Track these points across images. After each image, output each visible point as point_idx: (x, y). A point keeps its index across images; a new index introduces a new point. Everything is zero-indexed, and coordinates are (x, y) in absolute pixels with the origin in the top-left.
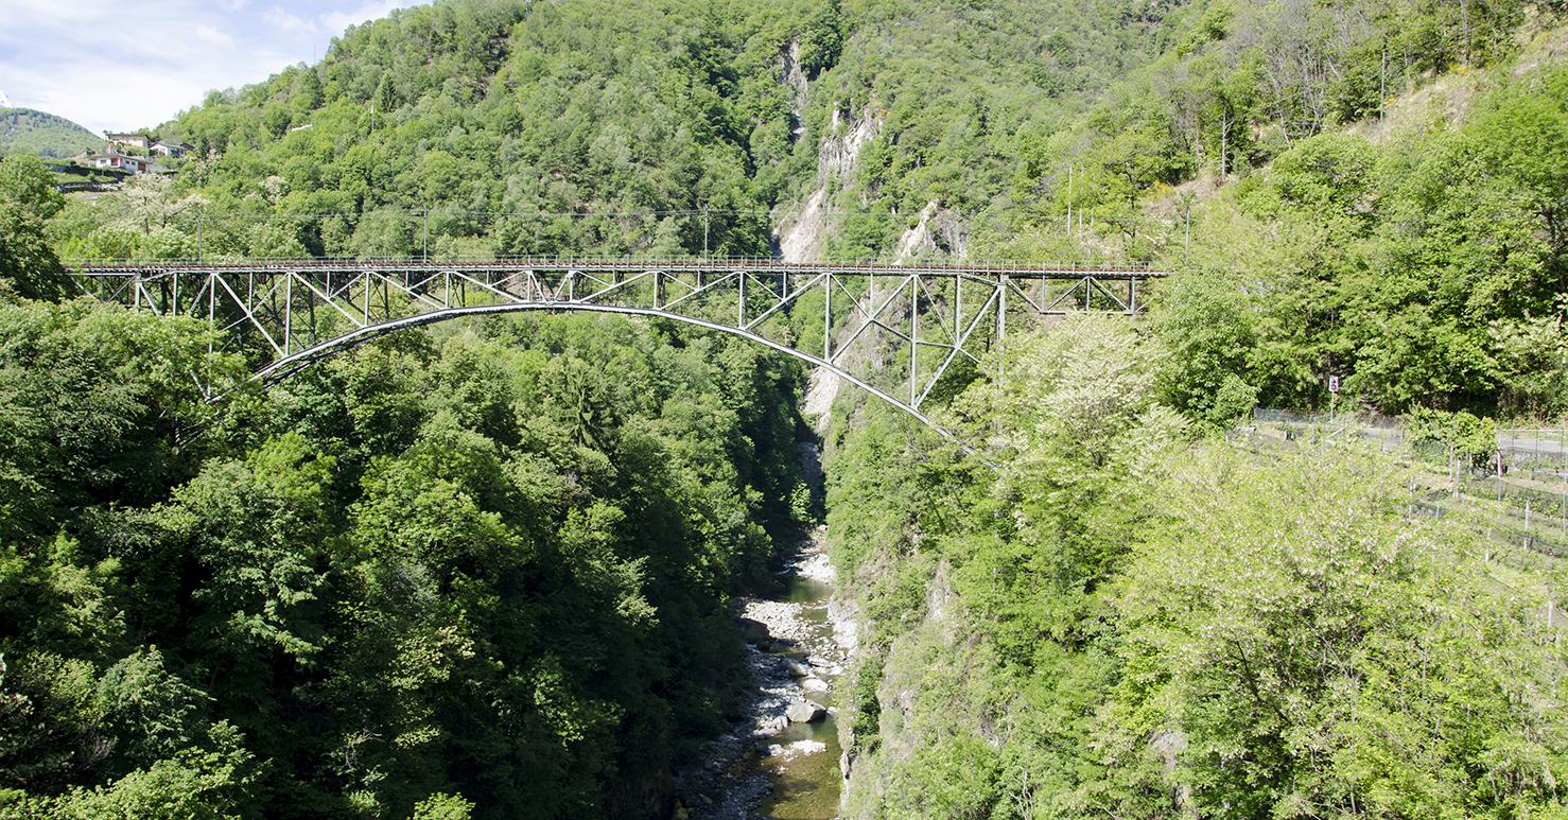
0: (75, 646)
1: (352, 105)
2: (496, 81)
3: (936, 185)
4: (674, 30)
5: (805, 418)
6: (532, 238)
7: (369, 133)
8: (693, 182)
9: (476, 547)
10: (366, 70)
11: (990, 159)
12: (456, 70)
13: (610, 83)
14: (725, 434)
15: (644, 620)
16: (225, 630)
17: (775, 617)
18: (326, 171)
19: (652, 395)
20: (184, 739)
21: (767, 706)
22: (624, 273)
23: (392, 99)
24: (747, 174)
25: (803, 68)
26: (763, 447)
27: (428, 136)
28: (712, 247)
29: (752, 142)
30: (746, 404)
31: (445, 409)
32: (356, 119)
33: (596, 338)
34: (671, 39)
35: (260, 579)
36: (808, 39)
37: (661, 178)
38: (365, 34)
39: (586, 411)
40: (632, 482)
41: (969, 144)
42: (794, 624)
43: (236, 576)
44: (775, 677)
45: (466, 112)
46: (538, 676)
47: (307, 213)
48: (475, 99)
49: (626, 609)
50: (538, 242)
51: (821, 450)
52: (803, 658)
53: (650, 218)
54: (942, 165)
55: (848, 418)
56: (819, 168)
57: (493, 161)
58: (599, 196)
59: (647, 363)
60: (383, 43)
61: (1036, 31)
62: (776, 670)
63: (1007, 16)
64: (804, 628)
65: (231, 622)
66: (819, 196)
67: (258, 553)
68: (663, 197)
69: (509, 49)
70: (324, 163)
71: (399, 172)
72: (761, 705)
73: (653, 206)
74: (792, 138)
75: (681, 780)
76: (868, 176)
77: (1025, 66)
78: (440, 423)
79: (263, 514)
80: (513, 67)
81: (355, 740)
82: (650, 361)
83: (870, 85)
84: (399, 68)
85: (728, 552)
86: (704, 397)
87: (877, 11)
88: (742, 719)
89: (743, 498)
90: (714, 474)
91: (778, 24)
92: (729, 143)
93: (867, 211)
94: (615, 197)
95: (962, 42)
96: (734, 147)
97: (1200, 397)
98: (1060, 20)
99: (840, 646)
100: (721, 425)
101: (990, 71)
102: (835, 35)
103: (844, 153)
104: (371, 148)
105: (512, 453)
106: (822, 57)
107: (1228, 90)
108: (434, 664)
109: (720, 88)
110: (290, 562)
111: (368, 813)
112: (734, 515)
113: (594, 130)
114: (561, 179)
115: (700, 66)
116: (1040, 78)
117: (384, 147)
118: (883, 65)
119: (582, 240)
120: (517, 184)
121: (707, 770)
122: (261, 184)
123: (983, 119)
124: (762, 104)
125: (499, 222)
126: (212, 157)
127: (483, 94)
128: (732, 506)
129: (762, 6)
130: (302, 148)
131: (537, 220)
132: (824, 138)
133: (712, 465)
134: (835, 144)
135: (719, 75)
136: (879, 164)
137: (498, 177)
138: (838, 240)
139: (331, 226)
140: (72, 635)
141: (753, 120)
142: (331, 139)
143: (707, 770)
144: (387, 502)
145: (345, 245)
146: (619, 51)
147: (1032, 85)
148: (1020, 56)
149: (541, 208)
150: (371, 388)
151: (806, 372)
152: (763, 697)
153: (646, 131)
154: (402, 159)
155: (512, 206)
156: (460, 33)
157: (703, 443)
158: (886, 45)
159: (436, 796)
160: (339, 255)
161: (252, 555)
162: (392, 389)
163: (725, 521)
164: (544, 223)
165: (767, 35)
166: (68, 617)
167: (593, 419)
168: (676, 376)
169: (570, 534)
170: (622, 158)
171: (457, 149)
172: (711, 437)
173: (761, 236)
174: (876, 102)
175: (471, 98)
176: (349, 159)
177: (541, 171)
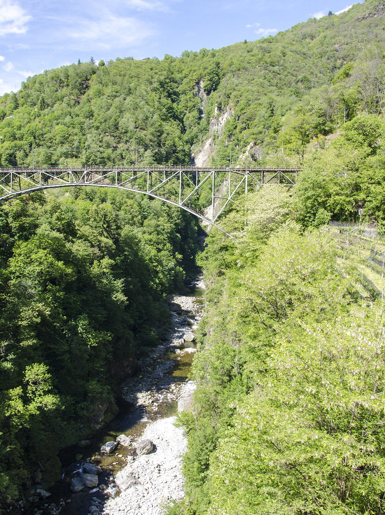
1: (28, 108)
2: (84, 98)
3: (253, 136)
5: (202, 227)
6: (96, 158)
7: (35, 118)
8: (159, 136)
9: (56, 274)
12: (68, 93)
14: (168, 233)
15: (123, 302)
18: (18, 134)
19: (140, 218)
23: (44, 105)
24: (182, 133)
25: (205, 91)
26: (185, 238)
27: (57, 120)
28: (167, 161)
29: (184, 120)
30: (177, 221)
31: (45, 223)
34: (153, 80)
36: (207, 79)
38: (34, 80)
39: (105, 224)
40: (125, 251)
41: (267, 120)
42: (192, 305)
45: (72, 110)
46: (80, 322)
47: (11, 150)
48: (76, 105)
49: (116, 298)
50: (99, 160)
52: (193, 317)
53: (142, 150)
54: (255, 128)
57: (82, 129)
58: (123, 142)
59: (138, 206)
60: (41, 83)
62: (182, 322)
63: (285, 69)
64: (195, 306)
66: (210, 141)
68: (147, 142)
69: (89, 85)
70: (18, 130)
71: (46, 134)
72: (175, 335)
73: (144, 146)
74: (200, 118)
77: (291, 89)
78: (43, 229)
80: (91, 92)
82: (139, 205)
83: (229, 97)
85: (167, 277)
86: (161, 219)
88: (167, 340)
89: (174, 257)
90: (163, 248)
91: (195, 73)
92: (175, 121)
94: (129, 142)
95: (266, 79)
97: (310, 217)
100: (167, 229)
101: (276, 91)
103: (219, 124)
104: (36, 124)
105: (74, 240)
106: (212, 86)
107: (346, 97)
108: (34, 317)
109: (172, 99)
111: (9, 370)
112: (170, 264)
113: (121, 116)
114: (108, 136)
115: (164, 91)
117: (41, 124)
118: (234, 89)
119: (116, 159)
120: (91, 137)
121: (151, 358)
123: (272, 110)
124: (189, 105)
125: (84, 152)
128: (170, 260)
129: (189, 66)
130: (9, 125)
131: (99, 151)
132: (211, 118)
133: (162, 245)
135: (172, 94)
136: (232, 128)
137: (84, 135)
138: (216, 158)
139: (19, 154)
141: (185, 111)
142: (20, 121)
143: (151, 358)
144: (21, 258)
145: (25, 162)
146: (132, 85)
147: (294, 96)
149: (100, 147)
151: (203, 209)
152: (175, 332)
153: (141, 116)
154: (47, 129)
155: (89, 147)
157: (159, 236)
159: (34, 364)
160: (23, 166)
162: (26, 216)
163: (167, 266)
164: (101, 153)
165: (191, 78)
167: (107, 227)
169: (95, 269)
171: (68, 124)
172: (162, 234)
173: (186, 156)
174: (231, 104)
175: (74, 104)
176: (27, 129)
177: (100, 132)
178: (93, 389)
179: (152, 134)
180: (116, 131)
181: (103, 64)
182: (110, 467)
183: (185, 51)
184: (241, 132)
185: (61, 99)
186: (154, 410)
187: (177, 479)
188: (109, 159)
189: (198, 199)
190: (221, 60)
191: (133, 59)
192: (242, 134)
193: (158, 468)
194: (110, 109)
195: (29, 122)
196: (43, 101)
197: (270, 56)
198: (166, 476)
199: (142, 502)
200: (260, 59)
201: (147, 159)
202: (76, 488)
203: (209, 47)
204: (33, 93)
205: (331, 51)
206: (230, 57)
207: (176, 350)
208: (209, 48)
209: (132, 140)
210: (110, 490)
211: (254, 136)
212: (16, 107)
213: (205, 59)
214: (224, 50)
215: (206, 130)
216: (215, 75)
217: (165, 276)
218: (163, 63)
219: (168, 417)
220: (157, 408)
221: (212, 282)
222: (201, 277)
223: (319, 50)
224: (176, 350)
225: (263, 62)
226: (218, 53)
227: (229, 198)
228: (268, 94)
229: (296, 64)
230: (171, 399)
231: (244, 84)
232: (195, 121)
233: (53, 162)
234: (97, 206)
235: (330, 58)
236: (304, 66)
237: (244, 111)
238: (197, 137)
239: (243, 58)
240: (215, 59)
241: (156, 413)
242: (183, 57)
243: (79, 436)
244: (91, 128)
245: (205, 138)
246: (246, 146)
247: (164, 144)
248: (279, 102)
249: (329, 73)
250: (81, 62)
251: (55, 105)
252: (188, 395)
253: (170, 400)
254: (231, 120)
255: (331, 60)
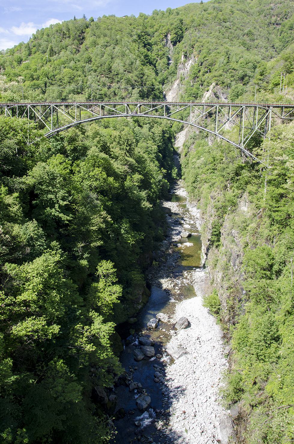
0: (13, 220)
1: (41, 55)
2: (83, 47)
5: (175, 148)
6: (96, 95)
7: (47, 63)
8: (142, 77)
10: (44, 44)
11: (231, 70)
13: (116, 47)
16: (44, 213)
17: (172, 206)
20: (45, 247)
21: (174, 232)
22: (116, 105)
25: (171, 42)
26: (164, 157)
28: (148, 97)
29: (157, 65)
32: (42, 59)
33: (118, 124)
34: (132, 33)
36: (173, 33)
37: (133, 76)
38: (42, 32)
39: (127, 146)
41: (224, 65)
44: (175, 224)
46: (122, 225)
49: (144, 205)
50: (98, 96)
51: (180, 157)
54: (216, 72)
56: (177, 73)
57: (83, 72)
58: (115, 82)
60: (48, 35)
61: (243, 29)
64: (180, 209)
66: (177, 82)
67: (53, 190)
68: (133, 82)
74: (168, 64)
76: (193, 75)
77: (239, 41)
79: (54, 179)
80: (88, 41)
82: (133, 131)
83: (193, 47)
84: (54, 43)
87: (195, 24)
88: (168, 236)
91: (164, 28)
92: (150, 66)
93: (193, 86)
94: (120, 82)
95: (221, 33)
96: (152, 67)
98: (250, 25)
99: (192, 215)
101: (229, 43)
102: (181, 32)
104: (47, 68)
106: (177, 39)
110: (61, 193)
114: (103, 77)
116: (244, 44)
117: (51, 68)
118: (197, 41)
120: (90, 78)
122: (17, 79)
123: (228, 58)
124: (160, 53)
127: (79, 51)
130: (27, 68)
132: (179, 64)
135: (146, 45)
137: (85, 76)
141: (157, 58)
146: (118, 37)
147: (242, 47)
150: (72, 140)
151: (175, 134)
152: (173, 230)
153: (128, 62)
154: (57, 71)
156: (71, 32)
158: (198, 34)
161: (51, 191)
165: (161, 32)
166: (10, 210)
168: (141, 136)
169: (127, 183)
171: (73, 68)
173: (161, 94)
174: (195, 53)
175: (75, 52)
181: (93, 21)
182: (159, 340)
183: (155, 10)
186: (177, 292)
187: (216, 349)
189: (171, 127)
190: (183, 17)
191: (115, 16)
192: (205, 77)
193: (198, 340)
195: (42, 66)
196: (52, 50)
198: (207, 347)
199: (195, 368)
200: (216, 17)
201: (135, 96)
202: (139, 357)
204: (43, 43)
205: (267, 10)
207: (178, 245)
209: (122, 81)
210: (165, 359)
212: (30, 55)
213: (171, 17)
214: (185, 10)
215: (174, 73)
216: (179, 30)
217: (157, 186)
219: (190, 298)
220: (179, 291)
222: (177, 187)
223: (258, 9)
226: (181, 12)
227: (256, 128)
229: (242, 20)
230: (187, 283)
231: (204, 37)
232: (165, 66)
233: (64, 98)
235: (266, 15)
236: (249, 22)
237: (206, 59)
238: (167, 78)
240: (179, 17)
241: (179, 295)
242: (153, 15)
243: (127, 315)
244: (90, 71)
245: (174, 79)
248: (234, 51)
249: (267, 27)
250: (76, 18)
252: (200, 281)
253: (186, 284)
254: (195, 65)
255: (267, 17)
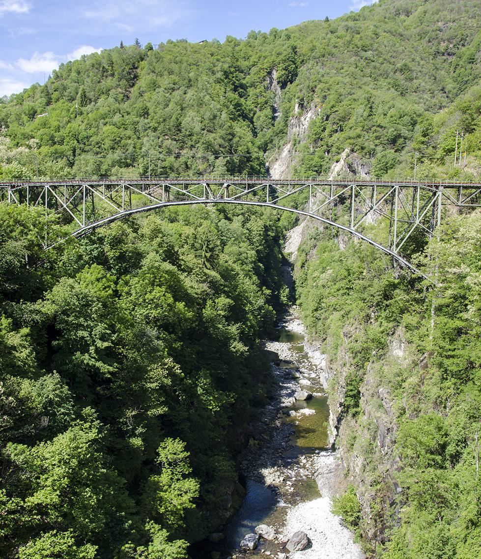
0: (21, 372)
1: (66, 103)
2: (134, 91)
4: (216, 64)
5: (285, 255)
7: (76, 117)
8: (231, 140)
10: (72, 86)
11: (375, 128)
13: (189, 91)
16: (71, 361)
17: (280, 349)
20: (73, 416)
25: (278, 83)
28: (241, 173)
29: (254, 120)
32: (69, 110)
34: (215, 69)
35: (87, 336)
36: (281, 68)
37: (216, 138)
38: (69, 68)
41: (365, 120)
43: (75, 335)
46: (199, 380)
49: (234, 348)
51: (293, 270)
53: (212, 158)
54: (352, 131)
55: (306, 254)
56: (288, 132)
57: (136, 131)
58: (187, 147)
60: (79, 73)
61: (394, 62)
63: (380, 54)
65: (74, 357)
66: (289, 146)
67: (86, 324)
68: (217, 147)
70: (56, 132)
73: (212, 152)
74: (274, 118)
75: (251, 428)
77: (388, 80)
79: (88, 305)
80: (142, 83)
81: (131, 413)
82: (217, 227)
83: (314, 91)
84: (87, 84)
87: (316, 53)
91: (266, 61)
92: (244, 121)
93: (313, 153)
94: (195, 147)
95: (358, 69)
96: (247, 123)
98: (406, 56)
100: (250, 258)
101: (372, 83)
104: (78, 125)
110: (100, 328)
112: (259, 301)
114: (168, 139)
116: (396, 86)
117: (84, 124)
118: (320, 81)
120: (147, 142)
122: (27, 143)
123: (371, 108)
125: (141, 160)
126: (3, 130)
127: (128, 97)
128: (258, 297)
130: (44, 124)
132: (291, 118)
134: (297, 121)
135: (238, 87)
137: (139, 138)
140: (19, 366)
141: (255, 109)
146: (192, 75)
147: (392, 90)
148: (386, 75)
150: (117, 242)
151: (285, 232)
152: (282, 388)
153: (208, 115)
156: (116, 67)
157: (244, 267)
158: (321, 70)
165: (261, 66)
166: (15, 357)
168: (229, 235)
169: (207, 312)
170: (197, 127)
172: (246, 264)
173: (262, 166)
174: (317, 100)
175: (123, 99)
176: (67, 130)
177: (159, 135)
178: (220, 466)
179: (222, 137)
180: (178, 134)
181: (151, 49)
183: (252, 31)
184: (331, 136)
185: (107, 92)
186: (290, 490)
188: (171, 168)
189: (279, 219)
190: (298, 43)
191: (187, 41)
192: (333, 138)
194: (170, 106)
195: (69, 122)
196: (84, 96)
197: (361, 37)
200: (350, 42)
201: (220, 169)
203: (282, 26)
205: (433, 31)
206: (309, 39)
207: (290, 412)
208: (281, 27)
209: (198, 145)
211: (351, 141)
212: (48, 103)
213: (278, 42)
214: (300, 31)
215: (282, 132)
217: (255, 317)
218: (225, 47)
219: (310, 501)
220: (292, 488)
221: (356, 328)
222: (289, 318)
223: (418, 29)
224: (290, 412)
225: (353, 46)
226: (293, 35)
227: (417, 222)
228: (363, 86)
229: (393, 48)
233: (104, 173)
234: (195, 229)
235: (431, 40)
236: (404, 51)
237: (335, 109)
238: (271, 141)
239: (327, 40)
240: (291, 42)
245: (283, 143)
246: (339, 153)
247: (236, 151)
248: (379, 97)
251: (100, 100)
254: (317, 120)
255: (433, 42)
